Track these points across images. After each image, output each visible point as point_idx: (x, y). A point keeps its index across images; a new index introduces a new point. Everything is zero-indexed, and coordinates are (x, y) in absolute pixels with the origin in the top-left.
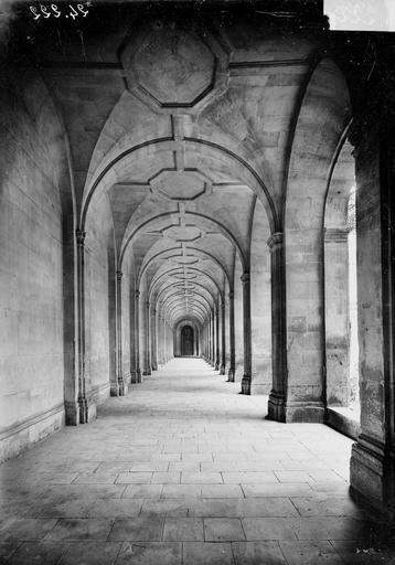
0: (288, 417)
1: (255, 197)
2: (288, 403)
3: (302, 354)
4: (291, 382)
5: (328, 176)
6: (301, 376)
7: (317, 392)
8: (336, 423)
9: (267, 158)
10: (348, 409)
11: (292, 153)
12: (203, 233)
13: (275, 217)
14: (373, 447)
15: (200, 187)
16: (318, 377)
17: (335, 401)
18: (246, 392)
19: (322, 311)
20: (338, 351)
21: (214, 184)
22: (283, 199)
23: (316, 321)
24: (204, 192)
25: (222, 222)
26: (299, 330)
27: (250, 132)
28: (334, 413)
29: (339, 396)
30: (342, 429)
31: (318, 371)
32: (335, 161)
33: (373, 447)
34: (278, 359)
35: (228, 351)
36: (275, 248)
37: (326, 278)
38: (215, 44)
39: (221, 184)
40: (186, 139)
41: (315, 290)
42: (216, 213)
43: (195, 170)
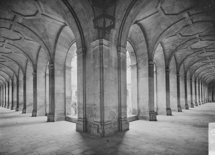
0: (55, 120)
1: (40, 47)
2: (55, 116)
3: (59, 101)
4: (56, 109)
5: (67, 52)
6: (59, 108)
7: (63, 112)
8: (68, 119)
9: (50, 41)
10: (71, 116)
11: (57, 43)
12: (13, 52)
13: (51, 59)
14: (119, 71)
15: (19, 38)
16: (64, 108)
17: (68, 114)
18: (34, 115)
19: (65, 89)
20: (69, 100)
21: (25, 39)
22: (54, 54)
23: (63, 92)
24: (20, 39)
25: (25, 51)
26: (58, 94)
27: (45, 31)
28: (68, 117)
29: (69, 112)
30: (70, 121)
31: (63, 106)
32: (69, 49)
33: (119, 71)
34: (51, 103)
35: (4, 100)
36: (50, 68)
37: (66, 80)
38: (37, 4)
39: (28, 40)
40: (18, 23)
41: (63, 83)
42: (23, 48)
43: (19, 32)
